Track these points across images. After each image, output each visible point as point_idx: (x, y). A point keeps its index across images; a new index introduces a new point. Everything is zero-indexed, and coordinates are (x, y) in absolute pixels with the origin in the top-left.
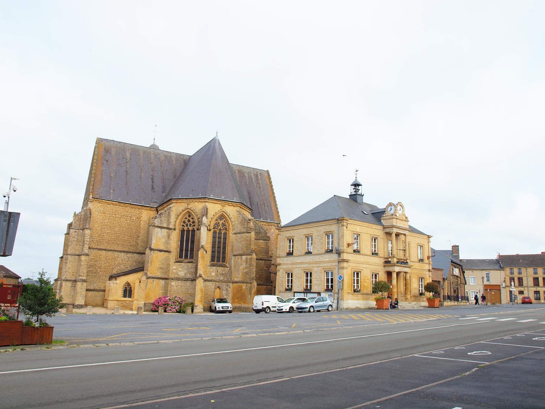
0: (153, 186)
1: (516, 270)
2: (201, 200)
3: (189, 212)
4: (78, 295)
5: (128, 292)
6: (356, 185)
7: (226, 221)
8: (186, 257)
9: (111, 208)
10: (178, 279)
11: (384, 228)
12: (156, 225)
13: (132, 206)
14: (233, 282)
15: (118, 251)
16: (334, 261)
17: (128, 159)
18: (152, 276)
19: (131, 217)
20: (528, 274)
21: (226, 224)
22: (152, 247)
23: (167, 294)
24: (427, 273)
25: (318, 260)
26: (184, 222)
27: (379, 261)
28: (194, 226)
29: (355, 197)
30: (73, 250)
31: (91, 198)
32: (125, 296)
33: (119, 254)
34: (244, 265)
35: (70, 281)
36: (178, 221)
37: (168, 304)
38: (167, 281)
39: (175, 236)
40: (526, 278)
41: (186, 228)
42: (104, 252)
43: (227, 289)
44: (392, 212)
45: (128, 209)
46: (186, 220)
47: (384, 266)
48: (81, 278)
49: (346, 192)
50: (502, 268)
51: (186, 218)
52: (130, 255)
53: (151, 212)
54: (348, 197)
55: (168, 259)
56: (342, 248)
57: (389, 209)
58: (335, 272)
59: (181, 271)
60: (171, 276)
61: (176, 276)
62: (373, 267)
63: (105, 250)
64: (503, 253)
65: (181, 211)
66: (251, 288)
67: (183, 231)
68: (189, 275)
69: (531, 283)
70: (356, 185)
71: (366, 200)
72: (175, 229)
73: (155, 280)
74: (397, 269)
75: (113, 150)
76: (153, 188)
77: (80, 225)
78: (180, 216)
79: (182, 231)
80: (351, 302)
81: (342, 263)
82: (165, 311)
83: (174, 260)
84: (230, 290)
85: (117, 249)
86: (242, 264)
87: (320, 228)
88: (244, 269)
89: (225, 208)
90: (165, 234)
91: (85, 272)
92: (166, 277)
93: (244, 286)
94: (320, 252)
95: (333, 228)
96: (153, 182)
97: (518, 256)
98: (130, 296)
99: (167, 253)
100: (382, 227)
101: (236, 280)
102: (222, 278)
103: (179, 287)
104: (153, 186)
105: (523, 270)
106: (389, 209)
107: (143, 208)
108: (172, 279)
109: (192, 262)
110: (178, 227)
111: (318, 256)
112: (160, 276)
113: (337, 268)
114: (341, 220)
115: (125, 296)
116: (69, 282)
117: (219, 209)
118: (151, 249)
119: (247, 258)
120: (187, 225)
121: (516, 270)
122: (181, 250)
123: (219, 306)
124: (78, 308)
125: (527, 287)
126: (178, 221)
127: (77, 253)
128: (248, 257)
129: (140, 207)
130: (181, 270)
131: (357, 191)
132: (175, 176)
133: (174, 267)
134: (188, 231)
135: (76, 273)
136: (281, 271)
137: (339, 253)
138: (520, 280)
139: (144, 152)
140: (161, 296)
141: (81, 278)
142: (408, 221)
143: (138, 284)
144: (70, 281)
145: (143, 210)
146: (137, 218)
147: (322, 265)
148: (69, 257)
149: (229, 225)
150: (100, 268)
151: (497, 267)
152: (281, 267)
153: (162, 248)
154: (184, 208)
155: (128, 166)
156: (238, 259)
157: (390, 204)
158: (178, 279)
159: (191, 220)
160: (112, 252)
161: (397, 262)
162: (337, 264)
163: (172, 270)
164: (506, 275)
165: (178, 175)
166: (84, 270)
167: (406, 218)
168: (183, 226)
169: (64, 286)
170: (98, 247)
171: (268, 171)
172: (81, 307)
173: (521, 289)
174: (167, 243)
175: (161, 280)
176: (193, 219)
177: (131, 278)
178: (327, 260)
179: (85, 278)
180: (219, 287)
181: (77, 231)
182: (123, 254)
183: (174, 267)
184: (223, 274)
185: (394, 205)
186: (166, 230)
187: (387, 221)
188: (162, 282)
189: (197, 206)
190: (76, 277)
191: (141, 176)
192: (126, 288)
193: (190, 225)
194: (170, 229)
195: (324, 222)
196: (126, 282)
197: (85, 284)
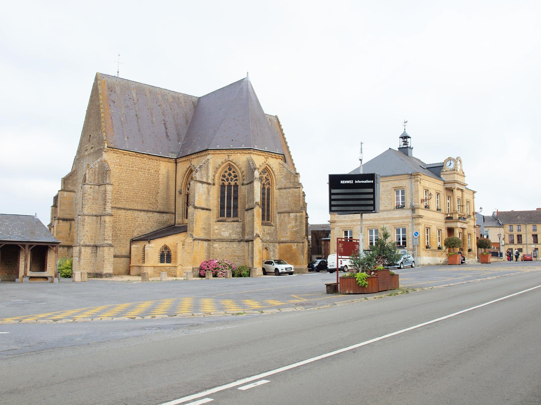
0: (167, 133)
1: (515, 227)
2: (245, 152)
3: (230, 165)
4: (106, 262)
5: (166, 256)
6: (405, 137)
7: (270, 174)
8: (229, 215)
9: (128, 160)
10: (222, 240)
11: (444, 183)
12: (197, 179)
13: (150, 157)
14: (280, 243)
15: (138, 210)
16: (406, 218)
17: (136, 101)
18: (197, 237)
19: (149, 170)
20: (527, 231)
21: (270, 178)
22: (196, 205)
23: (209, 257)
24: (473, 229)
25: (386, 216)
26: (224, 176)
27: (441, 217)
28: (236, 180)
29: (405, 150)
30: (90, 210)
31: (106, 147)
32: (162, 261)
33: (139, 213)
34: (293, 223)
35: (89, 246)
36: (217, 175)
37: (218, 268)
38: (209, 242)
39: (215, 191)
40: (525, 235)
41: (226, 183)
42: (123, 211)
43: (274, 250)
44: (452, 167)
45: (145, 160)
46: (226, 174)
47: (446, 222)
48: (106, 242)
49: (397, 144)
50: (501, 226)
51: (226, 172)
52: (150, 214)
53: (170, 164)
54: (398, 150)
55: (208, 218)
56: (417, 204)
57: (448, 164)
58: (409, 229)
59: (224, 231)
60: (212, 237)
61: (219, 237)
62: (438, 223)
63: (124, 209)
64: (500, 210)
65: (220, 163)
66: (303, 248)
67: (223, 186)
68: (234, 236)
69: (531, 239)
70: (405, 137)
71: (415, 154)
72: (214, 184)
73: (200, 241)
74: (459, 225)
75: (117, 89)
76: (167, 136)
77: (95, 180)
78: (220, 170)
79: (221, 186)
80: (425, 259)
81: (417, 219)
82: (215, 276)
83: (215, 219)
84: (277, 250)
85: (137, 208)
86: (289, 223)
87: (387, 183)
88: (293, 227)
89: (268, 160)
90: (206, 190)
91: (111, 235)
92: (208, 238)
93: (294, 246)
94: (389, 208)
95: (405, 183)
96: (166, 129)
97: (513, 212)
98: (169, 261)
99: (208, 211)
100: (443, 182)
101: (282, 239)
102: (268, 238)
103: (224, 249)
104: (167, 133)
105: (523, 227)
106: (448, 164)
107: (161, 159)
108: (215, 240)
109: (238, 221)
110: (218, 182)
111: (385, 213)
112: (203, 238)
113: (410, 225)
114: (414, 175)
115: (162, 261)
116: (89, 248)
117: (263, 162)
118: (196, 208)
119: (296, 216)
120: (228, 180)
121: (515, 227)
122: (222, 207)
123: (282, 268)
124: (107, 277)
125: (526, 244)
126: (217, 175)
127: (94, 213)
128: (298, 214)
129: (158, 158)
130: (228, 229)
131: (405, 143)
132: (187, 122)
133: (216, 227)
134: (229, 186)
135: (95, 237)
136: (337, 229)
137: (413, 209)
138: (519, 237)
139: (150, 92)
140: (205, 260)
141: (106, 242)
142: (464, 176)
143: (181, 246)
144: (89, 246)
145: (161, 162)
146: (156, 171)
147: (392, 222)
148: (86, 217)
149: (272, 179)
150: (120, 231)
151: (495, 224)
152: (336, 224)
153: (204, 206)
154: (223, 160)
155: (137, 110)
156: (284, 217)
157: (450, 159)
158: (222, 240)
159: (233, 174)
160: (131, 211)
161: (459, 218)
162: (411, 220)
163: (214, 230)
164: (505, 232)
165: (190, 120)
166: (109, 233)
167: (463, 173)
168: (223, 180)
169: (83, 252)
170: (117, 206)
171: (276, 117)
172: (110, 275)
173: (520, 246)
174: (207, 200)
175: (205, 242)
176: (234, 172)
177: (170, 241)
178: (397, 216)
179: (110, 242)
180: (266, 248)
181: (92, 187)
182: (143, 213)
183: (216, 227)
184: (269, 234)
185: (454, 160)
186: (205, 186)
187: (448, 176)
188: (206, 243)
189: (240, 159)
190: (95, 242)
191: (152, 120)
192: (163, 252)
193: (232, 179)
194: (209, 184)
195: (393, 177)
196: (163, 245)
197: (112, 249)
